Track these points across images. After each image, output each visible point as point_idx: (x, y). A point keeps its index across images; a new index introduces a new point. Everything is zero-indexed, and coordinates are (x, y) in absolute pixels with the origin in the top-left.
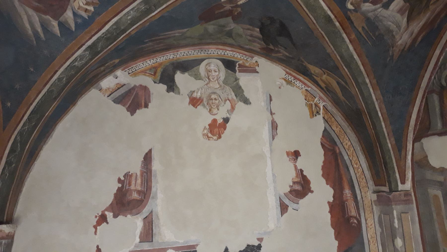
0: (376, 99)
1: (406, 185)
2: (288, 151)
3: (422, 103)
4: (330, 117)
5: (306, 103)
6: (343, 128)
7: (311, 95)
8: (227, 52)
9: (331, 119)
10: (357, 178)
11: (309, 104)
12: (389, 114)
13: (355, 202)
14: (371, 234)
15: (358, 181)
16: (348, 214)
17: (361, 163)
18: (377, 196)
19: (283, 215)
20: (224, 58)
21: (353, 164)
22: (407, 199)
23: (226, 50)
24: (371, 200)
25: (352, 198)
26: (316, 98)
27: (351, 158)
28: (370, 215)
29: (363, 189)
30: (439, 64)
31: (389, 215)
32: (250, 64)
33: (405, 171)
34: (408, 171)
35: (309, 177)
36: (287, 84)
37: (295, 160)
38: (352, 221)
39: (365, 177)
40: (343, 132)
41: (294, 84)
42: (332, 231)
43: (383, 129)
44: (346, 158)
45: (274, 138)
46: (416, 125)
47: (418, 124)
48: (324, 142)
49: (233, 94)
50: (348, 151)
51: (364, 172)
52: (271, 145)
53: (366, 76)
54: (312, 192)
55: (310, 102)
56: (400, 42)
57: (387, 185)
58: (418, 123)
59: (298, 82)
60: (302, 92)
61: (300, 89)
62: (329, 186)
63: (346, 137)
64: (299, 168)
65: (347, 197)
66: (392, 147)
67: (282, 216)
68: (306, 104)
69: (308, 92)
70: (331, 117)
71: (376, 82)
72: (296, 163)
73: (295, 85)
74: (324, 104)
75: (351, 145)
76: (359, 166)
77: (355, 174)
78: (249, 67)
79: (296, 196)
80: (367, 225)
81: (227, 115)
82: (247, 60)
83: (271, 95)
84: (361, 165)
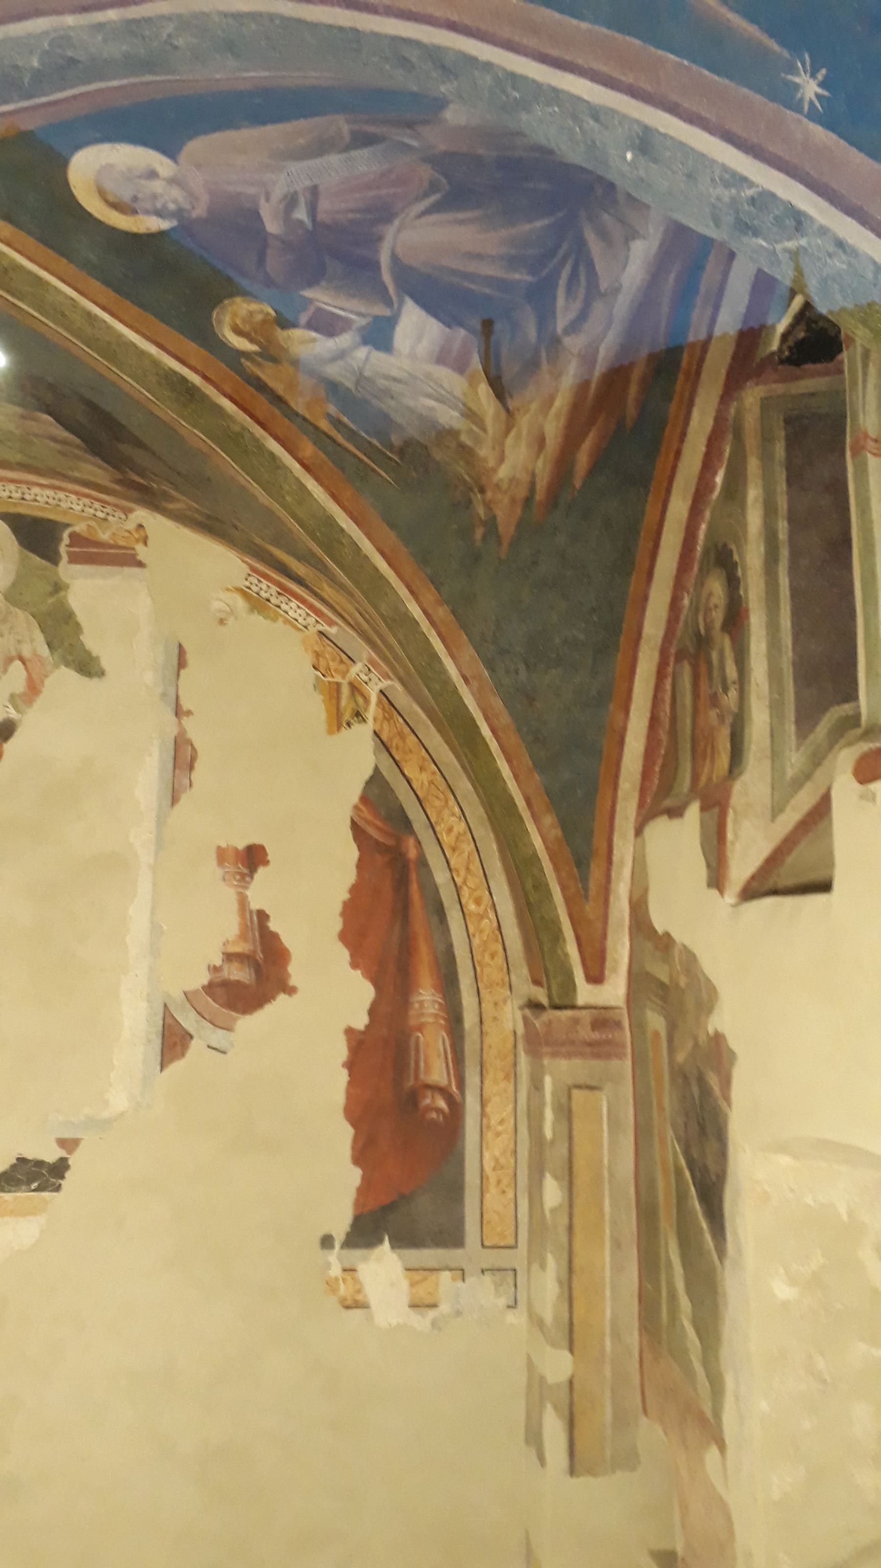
2: (224, 845)
5: (317, 678)
7: (337, 649)
8: (36, 490)
11: (329, 682)
12: (525, 729)
16: (417, 1077)
17: (495, 898)
18: (525, 1019)
20: (21, 510)
21: (464, 901)
22: (604, 1037)
23: (30, 484)
24: (515, 1033)
25: (442, 1022)
27: (459, 880)
28: (503, 1085)
29: (490, 992)
32: (114, 534)
33: (604, 936)
35: (287, 940)
37: (243, 876)
39: (505, 949)
40: (443, 785)
41: (278, 609)
44: (441, 877)
46: (646, 774)
51: (503, 931)
52: (161, 822)
53: (403, 592)
54: (291, 991)
56: (503, 473)
57: (545, 985)
59: (294, 604)
63: (452, 802)
64: (255, 905)
65: (422, 1015)
66: (547, 848)
68: (317, 686)
70: (407, 730)
72: (246, 888)
73: (282, 613)
75: (465, 833)
76: (486, 910)
78: (111, 547)
80: (485, 1121)
81: (7, 712)
82: (105, 520)
84: (494, 905)
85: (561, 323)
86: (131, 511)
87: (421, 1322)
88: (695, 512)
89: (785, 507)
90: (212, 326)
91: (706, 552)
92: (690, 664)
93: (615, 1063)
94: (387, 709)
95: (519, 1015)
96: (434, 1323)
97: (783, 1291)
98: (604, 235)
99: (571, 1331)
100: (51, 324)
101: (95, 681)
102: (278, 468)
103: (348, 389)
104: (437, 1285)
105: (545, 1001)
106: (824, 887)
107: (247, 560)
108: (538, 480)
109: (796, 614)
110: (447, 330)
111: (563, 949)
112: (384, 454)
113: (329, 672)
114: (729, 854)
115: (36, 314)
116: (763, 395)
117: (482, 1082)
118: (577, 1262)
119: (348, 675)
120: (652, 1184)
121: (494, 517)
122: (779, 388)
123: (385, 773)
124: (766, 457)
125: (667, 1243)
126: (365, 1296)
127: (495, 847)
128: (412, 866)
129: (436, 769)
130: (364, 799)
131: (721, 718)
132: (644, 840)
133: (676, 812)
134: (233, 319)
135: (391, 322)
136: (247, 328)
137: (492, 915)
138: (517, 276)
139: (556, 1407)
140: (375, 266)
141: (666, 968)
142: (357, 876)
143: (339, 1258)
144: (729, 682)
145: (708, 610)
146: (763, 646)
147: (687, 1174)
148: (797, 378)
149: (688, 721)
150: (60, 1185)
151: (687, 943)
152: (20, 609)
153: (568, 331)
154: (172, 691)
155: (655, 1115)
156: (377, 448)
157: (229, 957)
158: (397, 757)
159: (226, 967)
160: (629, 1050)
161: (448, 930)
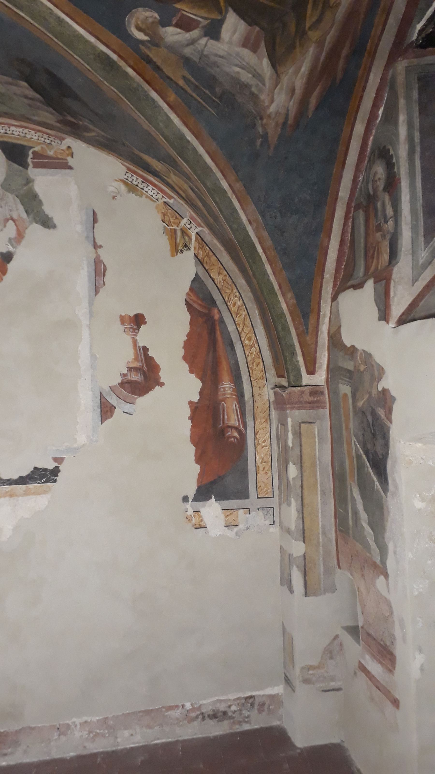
2: (123, 314)
3: (346, 228)
4: (207, 255)
5: (164, 227)
7: (174, 211)
8: (12, 128)
9: (209, 258)
10: (247, 363)
11: (171, 229)
12: (279, 248)
13: (239, 403)
14: (262, 456)
18: (275, 393)
19: (104, 422)
20: (5, 139)
21: (243, 339)
23: (10, 125)
24: (269, 400)
26: (183, 218)
27: (240, 329)
28: (264, 425)
29: (257, 382)
32: (55, 152)
34: (322, 352)
35: (158, 360)
36: (129, 191)
37: (134, 329)
38: (230, 434)
39: (263, 362)
40: (230, 282)
41: (142, 190)
43: (269, 276)
44: (231, 328)
45: (99, 292)
47: (343, 267)
49: (21, 208)
52: (91, 303)
53: (219, 175)
54: (162, 385)
55: (172, 226)
56: (272, 109)
57: (286, 377)
59: (150, 187)
60: (157, 208)
61: (153, 201)
62: (193, 375)
63: (235, 291)
64: (141, 344)
66: (289, 310)
67: (101, 424)
68: (165, 231)
70: (211, 253)
71: (243, 188)
72: (136, 336)
73: (145, 192)
74: (198, 231)
75: (242, 305)
76: (253, 343)
77: (245, 356)
79: (133, 393)
80: (256, 441)
81: (8, 248)
82: (50, 144)
83: (96, 211)
84: (257, 340)
86: (64, 139)
87: (231, 533)
88: (367, 131)
89: (418, 124)
90: (125, 24)
91: (372, 152)
92: (363, 211)
93: (321, 411)
94: (201, 243)
95: (272, 392)
96: (237, 534)
97: (419, 504)
100: (36, 25)
101: (51, 231)
103: (195, 61)
104: (237, 517)
105: (286, 384)
107: (126, 164)
108: (290, 112)
109: (424, 180)
110: (249, 28)
111: (296, 358)
113: (170, 223)
114: (391, 303)
115: (28, 18)
116: (406, 65)
117: (254, 424)
118: (305, 501)
120: (342, 465)
121: (267, 133)
122: (415, 61)
123: (201, 276)
124: (408, 98)
125: (351, 490)
126: (205, 523)
127: (257, 312)
128: (217, 323)
129: (226, 273)
130: (191, 289)
131: (384, 236)
132: (338, 302)
133: (359, 286)
135: (221, 22)
136: (143, 27)
137: (256, 345)
139: (298, 567)
141: (352, 363)
142: (190, 328)
143: (191, 506)
144: (388, 217)
145: (374, 181)
146: (408, 197)
147: (364, 457)
149: (362, 240)
150: (56, 479)
151: (366, 349)
152: (10, 193)
153: (310, 29)
154: (91, 235)
155: (344, 432)
157: (130, 369)
158: (207, 268)
159: (129, 374)
161: (236, 354)
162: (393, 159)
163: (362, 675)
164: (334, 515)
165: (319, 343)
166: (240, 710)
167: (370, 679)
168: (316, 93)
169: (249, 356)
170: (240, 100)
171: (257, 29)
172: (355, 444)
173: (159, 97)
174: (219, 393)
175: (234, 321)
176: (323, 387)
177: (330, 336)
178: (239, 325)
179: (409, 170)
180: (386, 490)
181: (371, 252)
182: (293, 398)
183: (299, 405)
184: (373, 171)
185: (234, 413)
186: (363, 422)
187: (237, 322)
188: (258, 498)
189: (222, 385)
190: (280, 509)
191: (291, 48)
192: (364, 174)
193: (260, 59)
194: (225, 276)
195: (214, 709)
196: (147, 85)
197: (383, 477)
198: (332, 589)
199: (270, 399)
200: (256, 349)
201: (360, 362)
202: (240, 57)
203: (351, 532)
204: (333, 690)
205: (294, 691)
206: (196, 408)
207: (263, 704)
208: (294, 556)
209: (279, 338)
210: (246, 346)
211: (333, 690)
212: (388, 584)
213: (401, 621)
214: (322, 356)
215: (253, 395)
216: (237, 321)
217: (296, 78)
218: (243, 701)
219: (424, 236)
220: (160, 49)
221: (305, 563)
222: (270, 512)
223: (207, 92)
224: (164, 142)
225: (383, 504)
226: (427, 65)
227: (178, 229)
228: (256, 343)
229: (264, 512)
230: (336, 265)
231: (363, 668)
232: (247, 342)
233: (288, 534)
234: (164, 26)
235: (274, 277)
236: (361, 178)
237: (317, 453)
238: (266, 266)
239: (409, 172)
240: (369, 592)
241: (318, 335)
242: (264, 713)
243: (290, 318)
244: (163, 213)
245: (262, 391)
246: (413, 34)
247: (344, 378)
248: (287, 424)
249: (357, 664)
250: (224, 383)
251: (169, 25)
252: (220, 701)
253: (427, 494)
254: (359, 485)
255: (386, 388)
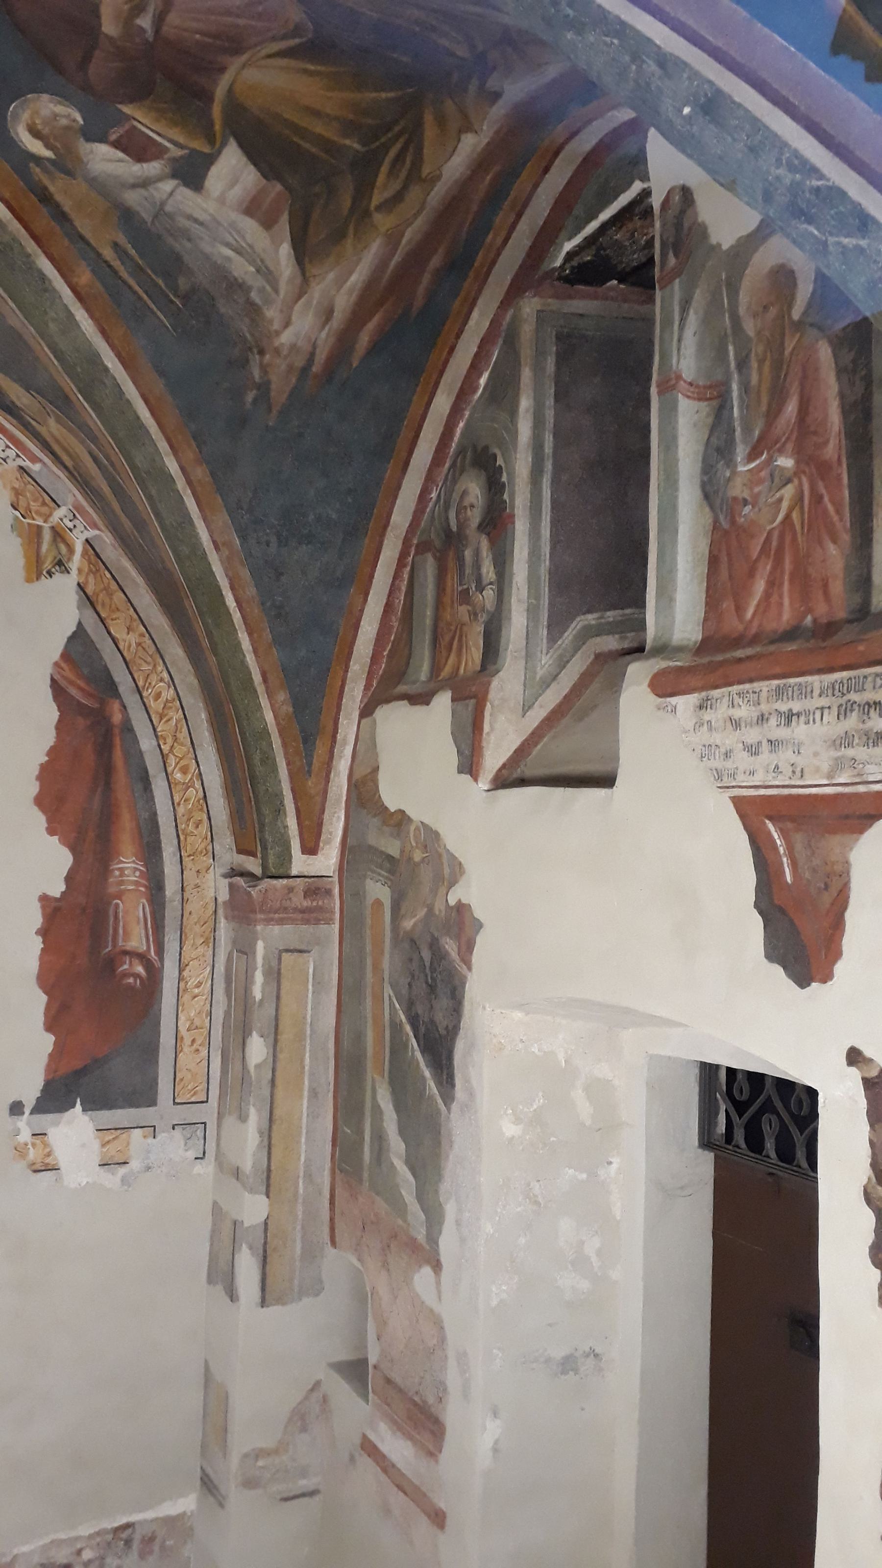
0: (215, 543)
1: (320, 857)
3: (397, 582)
6: (154, 637)
9: (110, 595)
10: (176, 820)
11: (29, 524)
12: (268, 604)
15: (177, 831)
18: (231, 886)
21: (170, 769)
22: (315, 904)
24: (216, 899)
25: (142, 889)
26: (59, 506)
27: (166, 748)
28: (201, 950)
29: (193, 859)
30: (452, 450)
31: (247, 955)
33: (323, 811)
34: (335, 813)
39: (209, 819)
42: (778, 971)
43: (244, 656)
44: (146, 744)
46: (375, 658)
47: (385, 653)
48: (64, 677)
50: (158, 720)
53: (163, 445)
55: (34, 519)
56: (286, 338)
57: (259, 855)
58: (384, 650)
66: (278, 724)
68: (16, 527)
69: (30, 480)
71: (209, 479)
75: (174, 700)
76: (191, 779)
77: (173, 804)
80: (182, 985)
84: (200, 774)
85: (377, 199)
87: (111, 1179)
89: (552, 421)
90: (6, 118)
91: (461, 451)
94: (93, 562)
95: (224, 884)
96: (124, 1181)
97: (510, 1129)
98: (441, 121)
99: (268, 1178)
102: (46, 290)
104: (128, 1144)
105: (258, 871)
106: (607, 781)
108: (318, 351)
110: (264, 181)
112: (167, 296)
114: (484, 744)
117: (181, 949)
118: (278, 1112)
119: (51, 519)
120: (359, 1038)
121: (269, 382)
122: (554, 304)
123: (89, 630)
124: (538, 369)
126: (56, 1159)
128: (116, 731)
131: (474, 615)
132: (375, 721)
133: (421, 699)
134: (32, 118)
135: (210, 160)
136: (46, 131)
137: (198, 785)
138: (348, 142)
140: (207, 97)
141: (397, 843)
143: (29, 1124)
146: (525, 553)
147: (408, 1028)
148: (570, 297)
151: (426, 821)
153: (378, 208)
156: (160, 287)
158: (103, 615)
160: (337, 916)
161: (152, 798)
162: (501, 476)
163: (365, 1462)
164: (331, 1139)
165: (331, 795)
166: (102, 1558)
167: (385, 1470)
168: (371, 326)
169: (181, 806)
170: (223, 310)
171: (279, 187)
172: (391, 1005)
173: (56, 272)
174: (111, 880)
175: (154, 729)
176: (332, 882)
177: (353, 782)
178: (165, 739)
179: (531, 502)
180: (448, 1094)
181: (447, 638)
182: (272, 901)
183: (281, 915)
184: (460, 487)
185: (138, 923)
186: (411, 960)
187: (159, 734)
188: (175, 1103)
189: (117, 864)
190: (219, 1126)
191: (338, 236)
192: (441, 489)
193: (277, 245)
194: (142, 635)
195: (45, 1561)
196: (33, 243)
197: (445, 1073)
198: (315, 1288)
199: (217, 897)
200: (197, 793)
201: (414, 844)
202: (238, 232)
203: (366, 1175)
204: (303, 1495)
205: (221, 1505)
206: (57, 910)
207: (152, 1539)
208: (246, 1225)
209: (253, 778)
210: (176, 784)
211: (303, 1495)
212: (438, 1283)
213: (462, 1357)
214: (334, 819)
215: (182, 886)
216: (160, 732)
217: (338, 291)
218: (110, 1537)
219: (549, 626)
220: (74, 181)
221: (266, 1237)
222: (198, 1132)
223: (160, 282)
224: (47, 354)
225: (440, 1125)
226: (573, 314)
227: (46, 526)
228: (198, 780)
229: (184, 1132)
230: (374, 650)
231: (370, 1449)
232: (178, 776)
233: (234, 1180)
234: (88, 139)
235: (254, 658)
236: (434, 495)
237: (309, 1012)
238: (240, 635)
239: (530, 506)
240: (396, 1297)
241: (329, 778)
242: (151, 1559)
243: (279, 741)
244: (14, 488)
245: (204, 881)
246: (557, 257)
247: (379, 870)
248: (254, 953)
249: (358, 1441)
250: (122, 859)
251: (102, 140)
252: (55, 1543)
253: (526, 1109)
254: (392, 1082)
255: (464, 901)
